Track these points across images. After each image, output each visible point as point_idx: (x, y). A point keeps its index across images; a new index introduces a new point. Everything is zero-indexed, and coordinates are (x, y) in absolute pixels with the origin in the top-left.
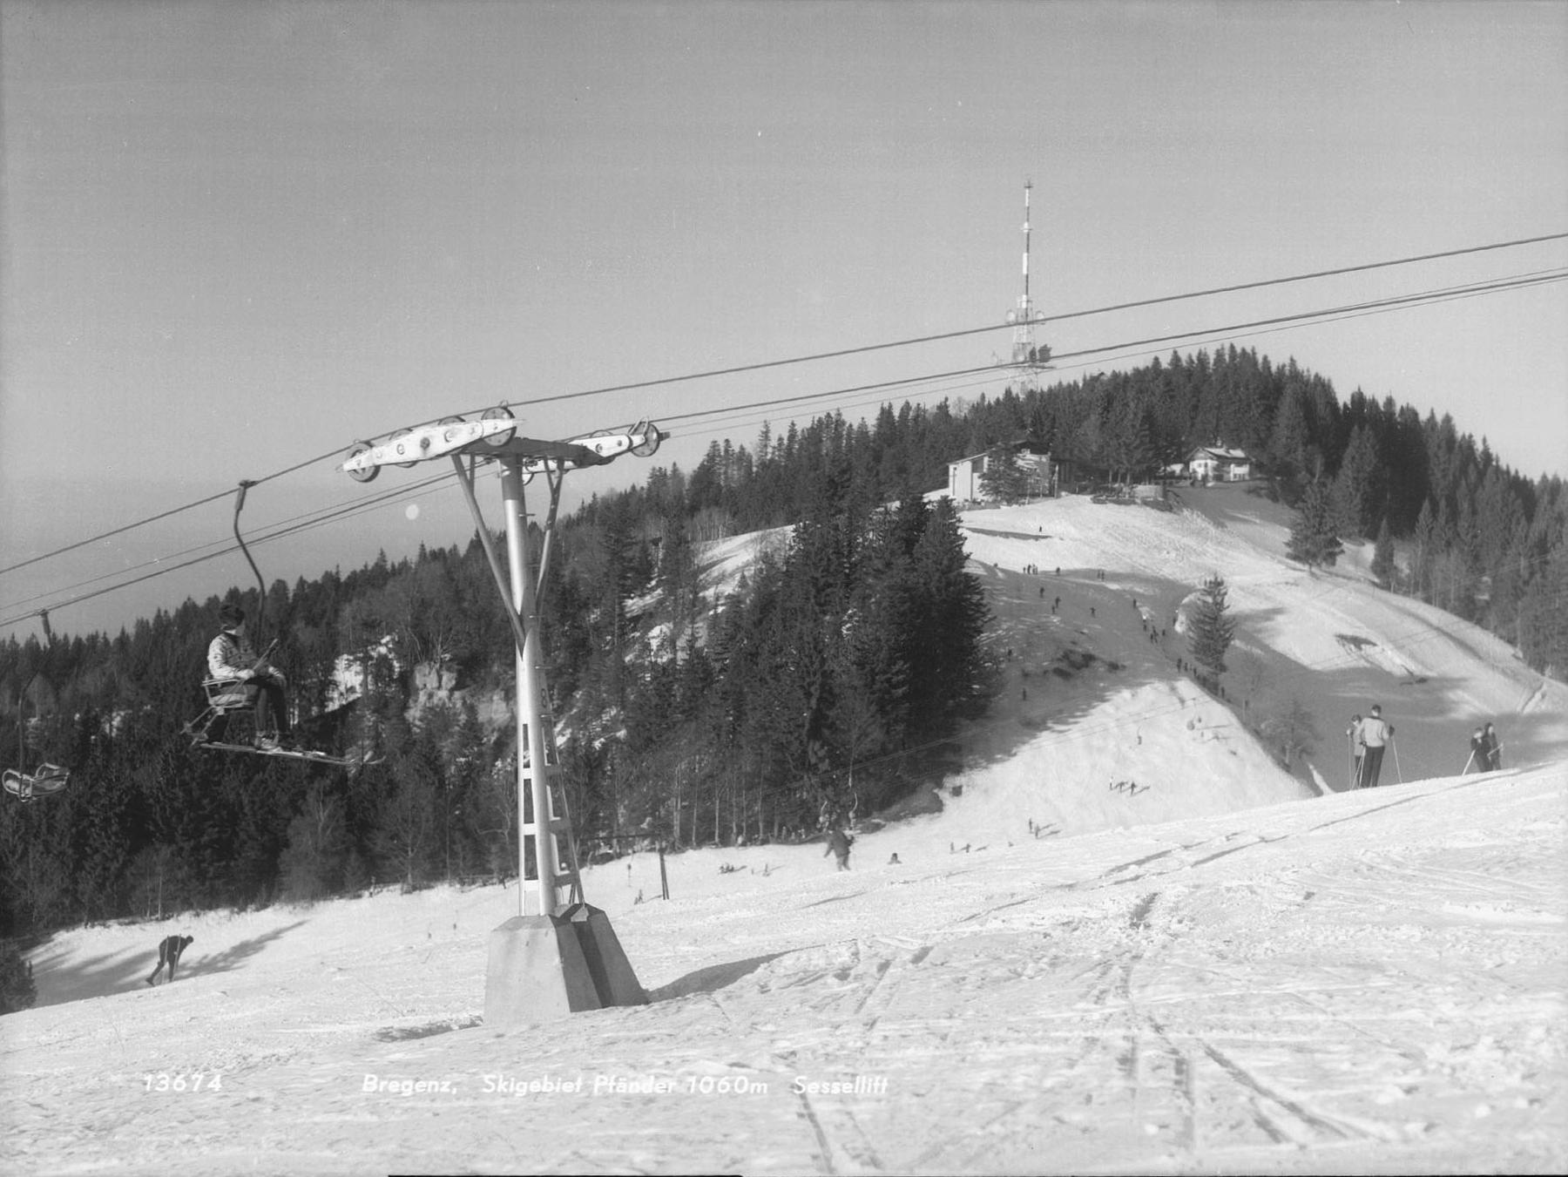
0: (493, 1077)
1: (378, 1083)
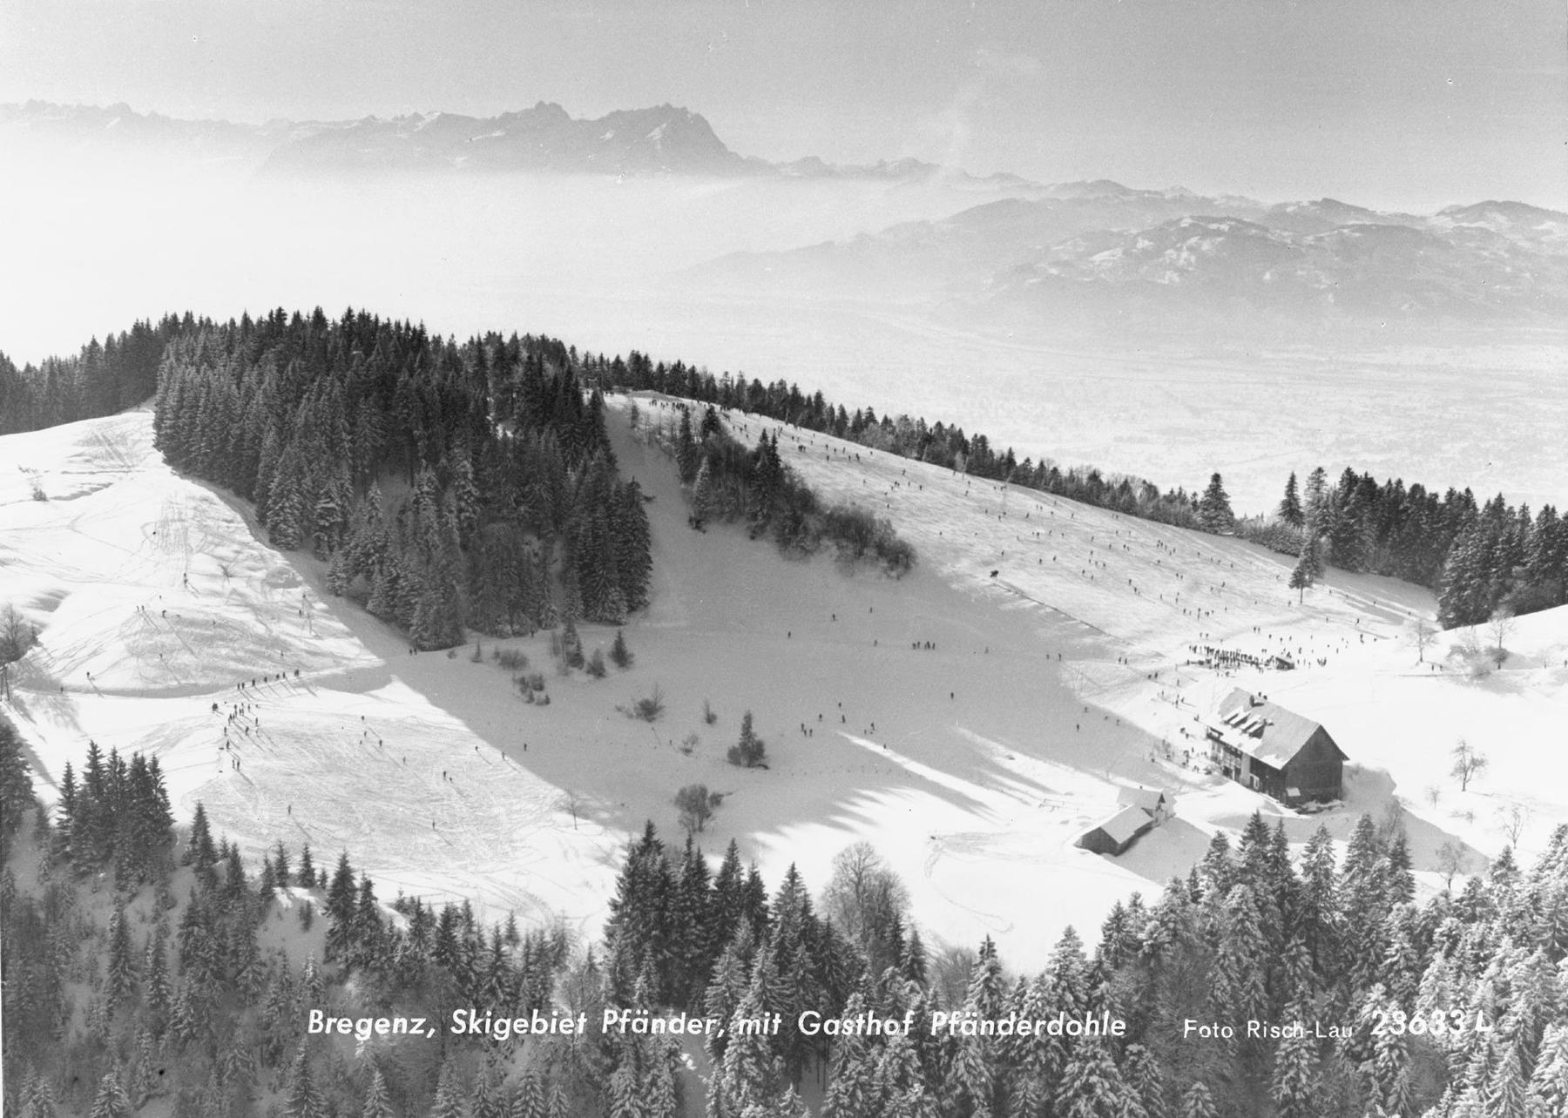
0: (464, 1013)
1: (324, 1021)
